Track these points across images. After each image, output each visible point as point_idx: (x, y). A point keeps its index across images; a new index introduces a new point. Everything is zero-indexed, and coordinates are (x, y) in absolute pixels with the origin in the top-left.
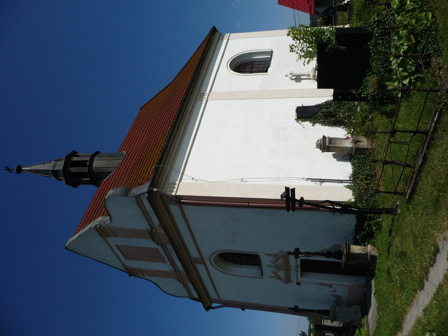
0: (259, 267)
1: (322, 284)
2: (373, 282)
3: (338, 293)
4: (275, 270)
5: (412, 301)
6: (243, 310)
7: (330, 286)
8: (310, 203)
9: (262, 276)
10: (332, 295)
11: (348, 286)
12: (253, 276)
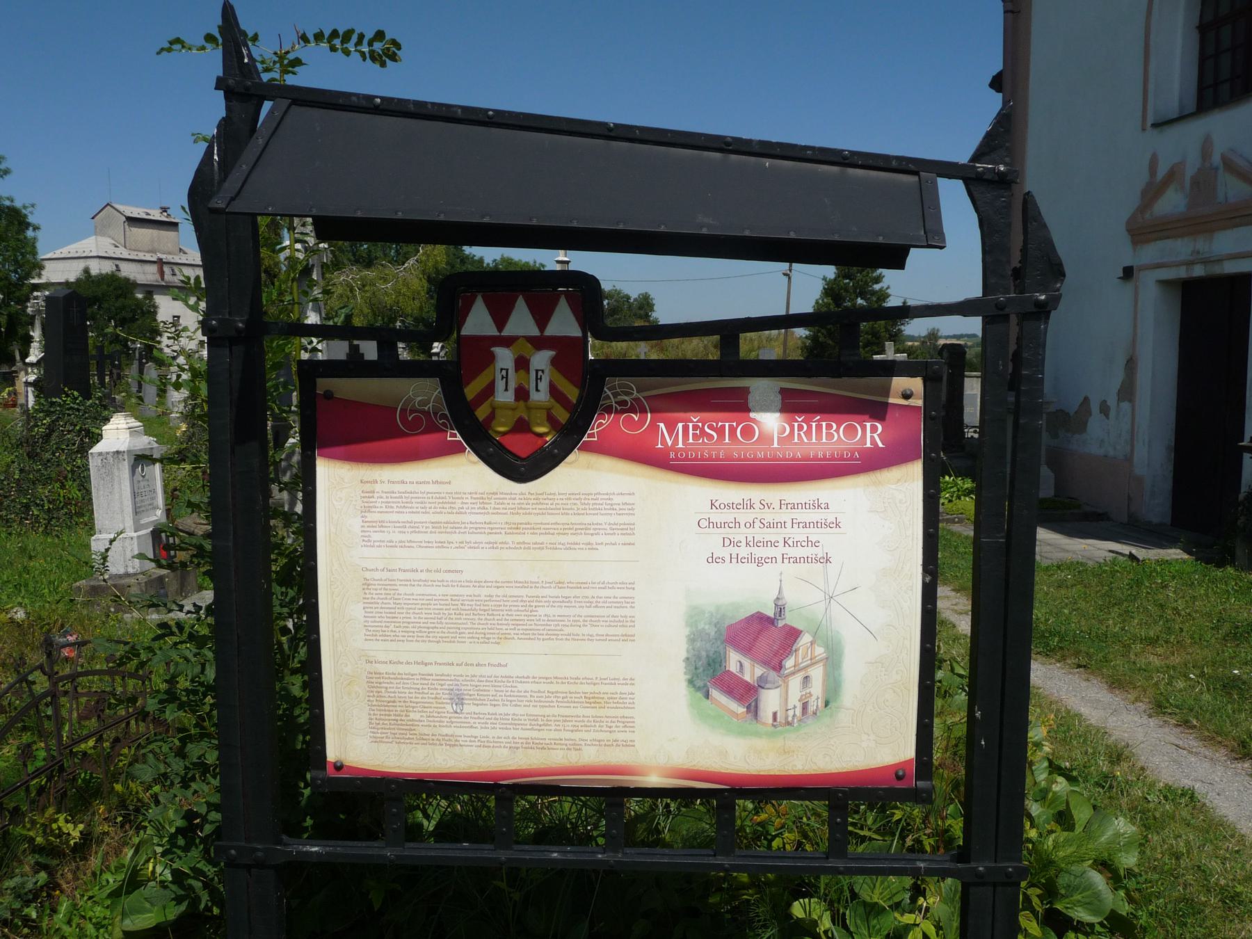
0: (1191, 106)
1: (1131, 365)
2: (1175, 554)
3: (1096, 424)
4: (1190, 171)
5: (1185, 724)
6: (997, 83)
7: (1127, 392)
8: (916, 308)
9: (1155, 125)
10: (1086, 399)
11: (1129, 459)
12: (1151, 87)
